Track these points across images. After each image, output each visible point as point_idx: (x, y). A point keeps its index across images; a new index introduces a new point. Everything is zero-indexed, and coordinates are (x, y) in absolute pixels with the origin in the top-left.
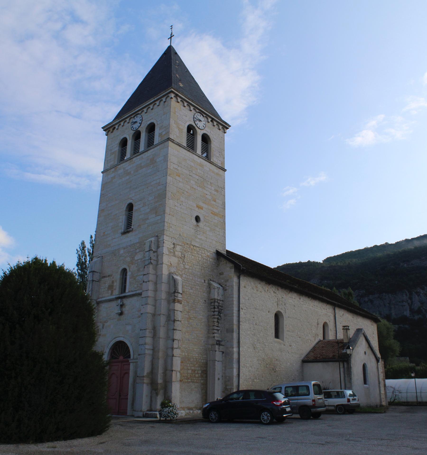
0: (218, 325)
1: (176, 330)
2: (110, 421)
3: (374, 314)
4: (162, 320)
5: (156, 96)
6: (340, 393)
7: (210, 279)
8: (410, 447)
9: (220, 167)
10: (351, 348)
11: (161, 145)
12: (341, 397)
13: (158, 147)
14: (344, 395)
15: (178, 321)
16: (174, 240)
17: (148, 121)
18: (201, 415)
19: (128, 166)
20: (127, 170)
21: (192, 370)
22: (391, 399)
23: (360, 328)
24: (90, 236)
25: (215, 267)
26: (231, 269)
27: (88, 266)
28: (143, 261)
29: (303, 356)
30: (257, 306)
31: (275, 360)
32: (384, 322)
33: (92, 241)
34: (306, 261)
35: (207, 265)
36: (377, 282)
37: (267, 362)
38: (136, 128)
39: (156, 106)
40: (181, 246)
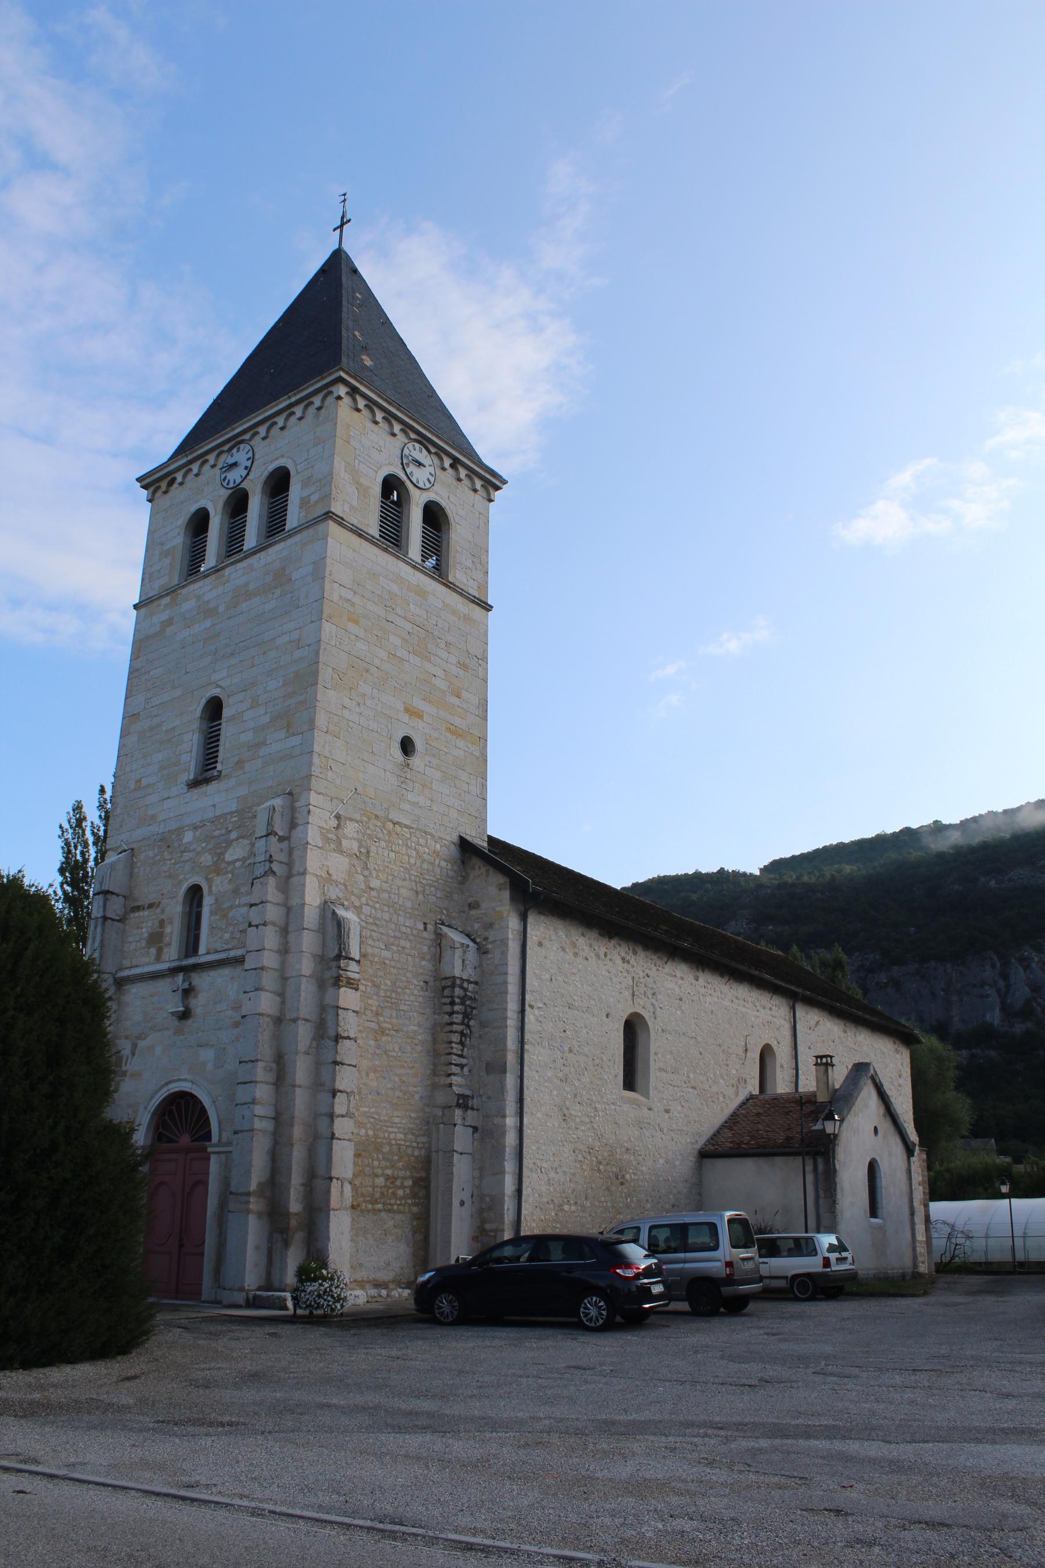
0: (462, 1050)
1: (343, 1064)
2: (152, 1316)
3: (903, 1021)
4: (303, 1034)
5: (295, 391)
6: (803, 1242)
7: (440, 920)
8: (991, 1392)
9: (475, 597)
10: (836, 1117)
11: (305, 533)
12: (805, 1252)
13: (297, 538)
14: (813, 1248)
15: (348, 1038)
16: (337, 806)
17: (271, 462)
18: (413, 1302)
19: (211, 590)
20: (208, 602)
21: (387, 1178)
22: (943, 1256)
23: (865, 1061)
24: (99, 788)
25: (455, 885)
26: (500, 889)
27: (92, 874)
28: (250, 864)
29: (702, 1141)
30: (576, 999)
31: (624, 1150)
32: (930, 1041)
33: (105, 803)
34: (714, 869)
35: (432, 878)
36: (912, 929)
37: (599, 1157)
38: (235, 482)
39: (293, 420)
40: (357, 822)
